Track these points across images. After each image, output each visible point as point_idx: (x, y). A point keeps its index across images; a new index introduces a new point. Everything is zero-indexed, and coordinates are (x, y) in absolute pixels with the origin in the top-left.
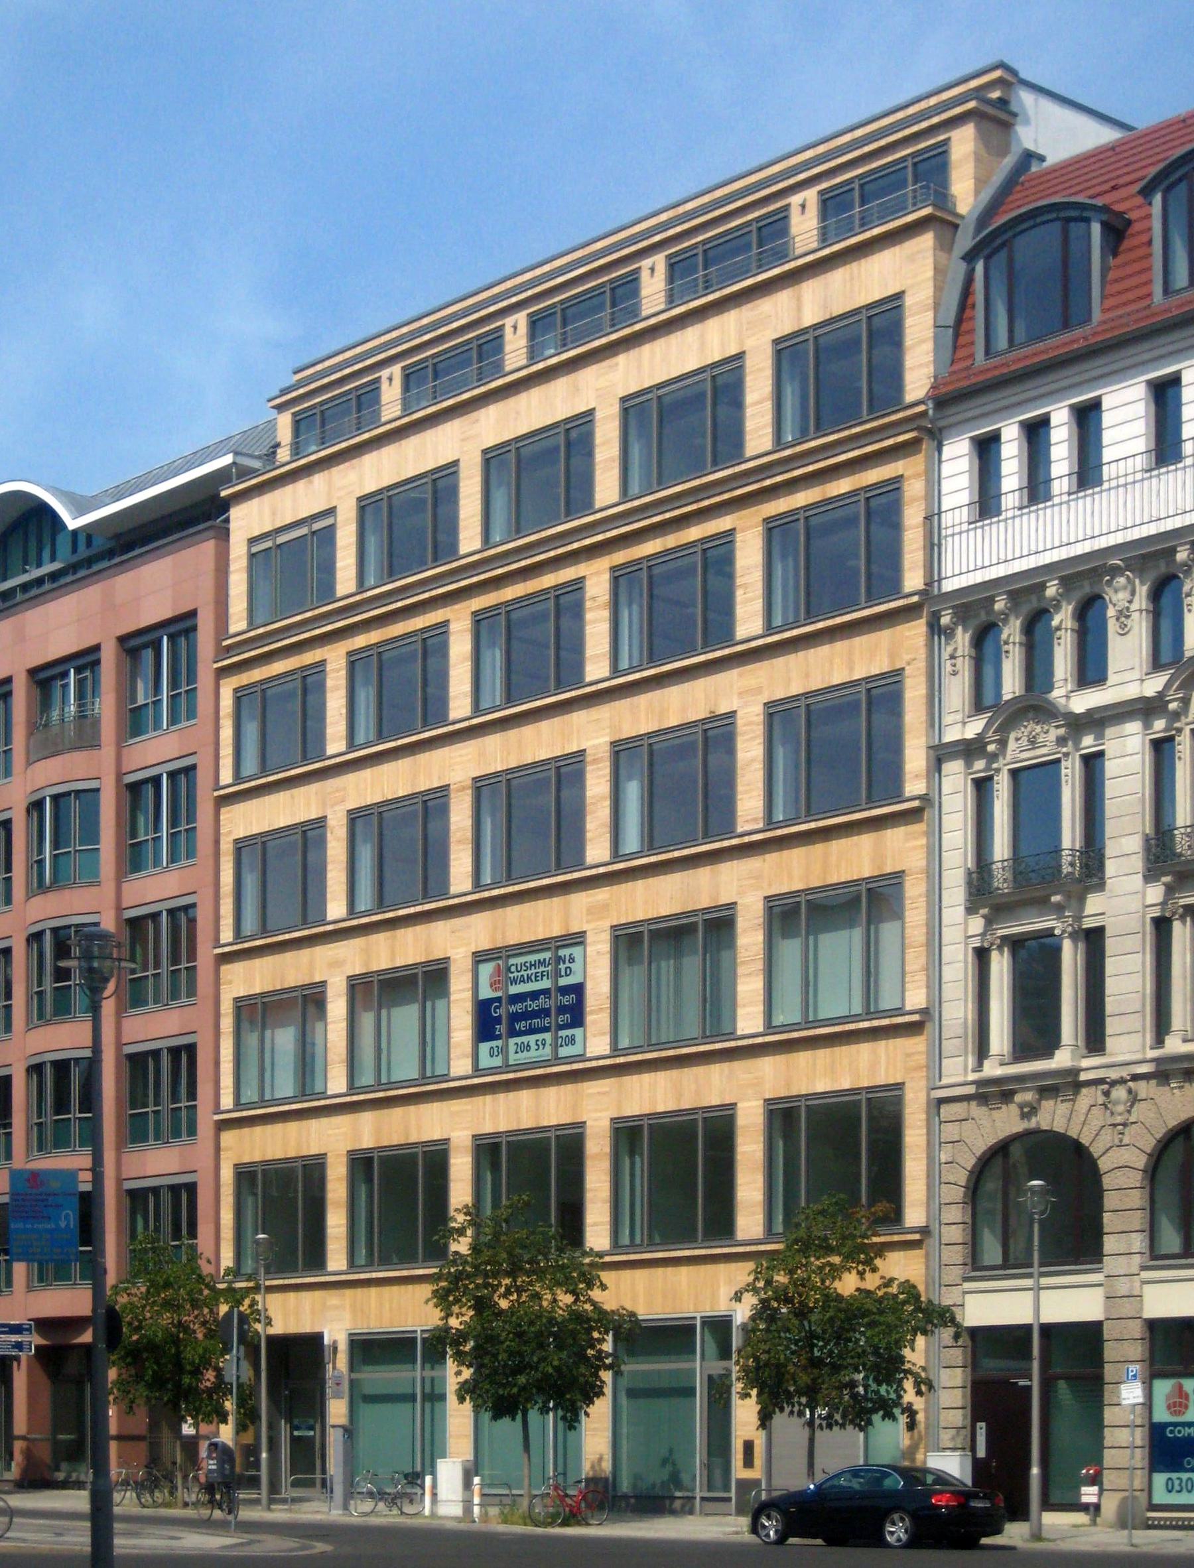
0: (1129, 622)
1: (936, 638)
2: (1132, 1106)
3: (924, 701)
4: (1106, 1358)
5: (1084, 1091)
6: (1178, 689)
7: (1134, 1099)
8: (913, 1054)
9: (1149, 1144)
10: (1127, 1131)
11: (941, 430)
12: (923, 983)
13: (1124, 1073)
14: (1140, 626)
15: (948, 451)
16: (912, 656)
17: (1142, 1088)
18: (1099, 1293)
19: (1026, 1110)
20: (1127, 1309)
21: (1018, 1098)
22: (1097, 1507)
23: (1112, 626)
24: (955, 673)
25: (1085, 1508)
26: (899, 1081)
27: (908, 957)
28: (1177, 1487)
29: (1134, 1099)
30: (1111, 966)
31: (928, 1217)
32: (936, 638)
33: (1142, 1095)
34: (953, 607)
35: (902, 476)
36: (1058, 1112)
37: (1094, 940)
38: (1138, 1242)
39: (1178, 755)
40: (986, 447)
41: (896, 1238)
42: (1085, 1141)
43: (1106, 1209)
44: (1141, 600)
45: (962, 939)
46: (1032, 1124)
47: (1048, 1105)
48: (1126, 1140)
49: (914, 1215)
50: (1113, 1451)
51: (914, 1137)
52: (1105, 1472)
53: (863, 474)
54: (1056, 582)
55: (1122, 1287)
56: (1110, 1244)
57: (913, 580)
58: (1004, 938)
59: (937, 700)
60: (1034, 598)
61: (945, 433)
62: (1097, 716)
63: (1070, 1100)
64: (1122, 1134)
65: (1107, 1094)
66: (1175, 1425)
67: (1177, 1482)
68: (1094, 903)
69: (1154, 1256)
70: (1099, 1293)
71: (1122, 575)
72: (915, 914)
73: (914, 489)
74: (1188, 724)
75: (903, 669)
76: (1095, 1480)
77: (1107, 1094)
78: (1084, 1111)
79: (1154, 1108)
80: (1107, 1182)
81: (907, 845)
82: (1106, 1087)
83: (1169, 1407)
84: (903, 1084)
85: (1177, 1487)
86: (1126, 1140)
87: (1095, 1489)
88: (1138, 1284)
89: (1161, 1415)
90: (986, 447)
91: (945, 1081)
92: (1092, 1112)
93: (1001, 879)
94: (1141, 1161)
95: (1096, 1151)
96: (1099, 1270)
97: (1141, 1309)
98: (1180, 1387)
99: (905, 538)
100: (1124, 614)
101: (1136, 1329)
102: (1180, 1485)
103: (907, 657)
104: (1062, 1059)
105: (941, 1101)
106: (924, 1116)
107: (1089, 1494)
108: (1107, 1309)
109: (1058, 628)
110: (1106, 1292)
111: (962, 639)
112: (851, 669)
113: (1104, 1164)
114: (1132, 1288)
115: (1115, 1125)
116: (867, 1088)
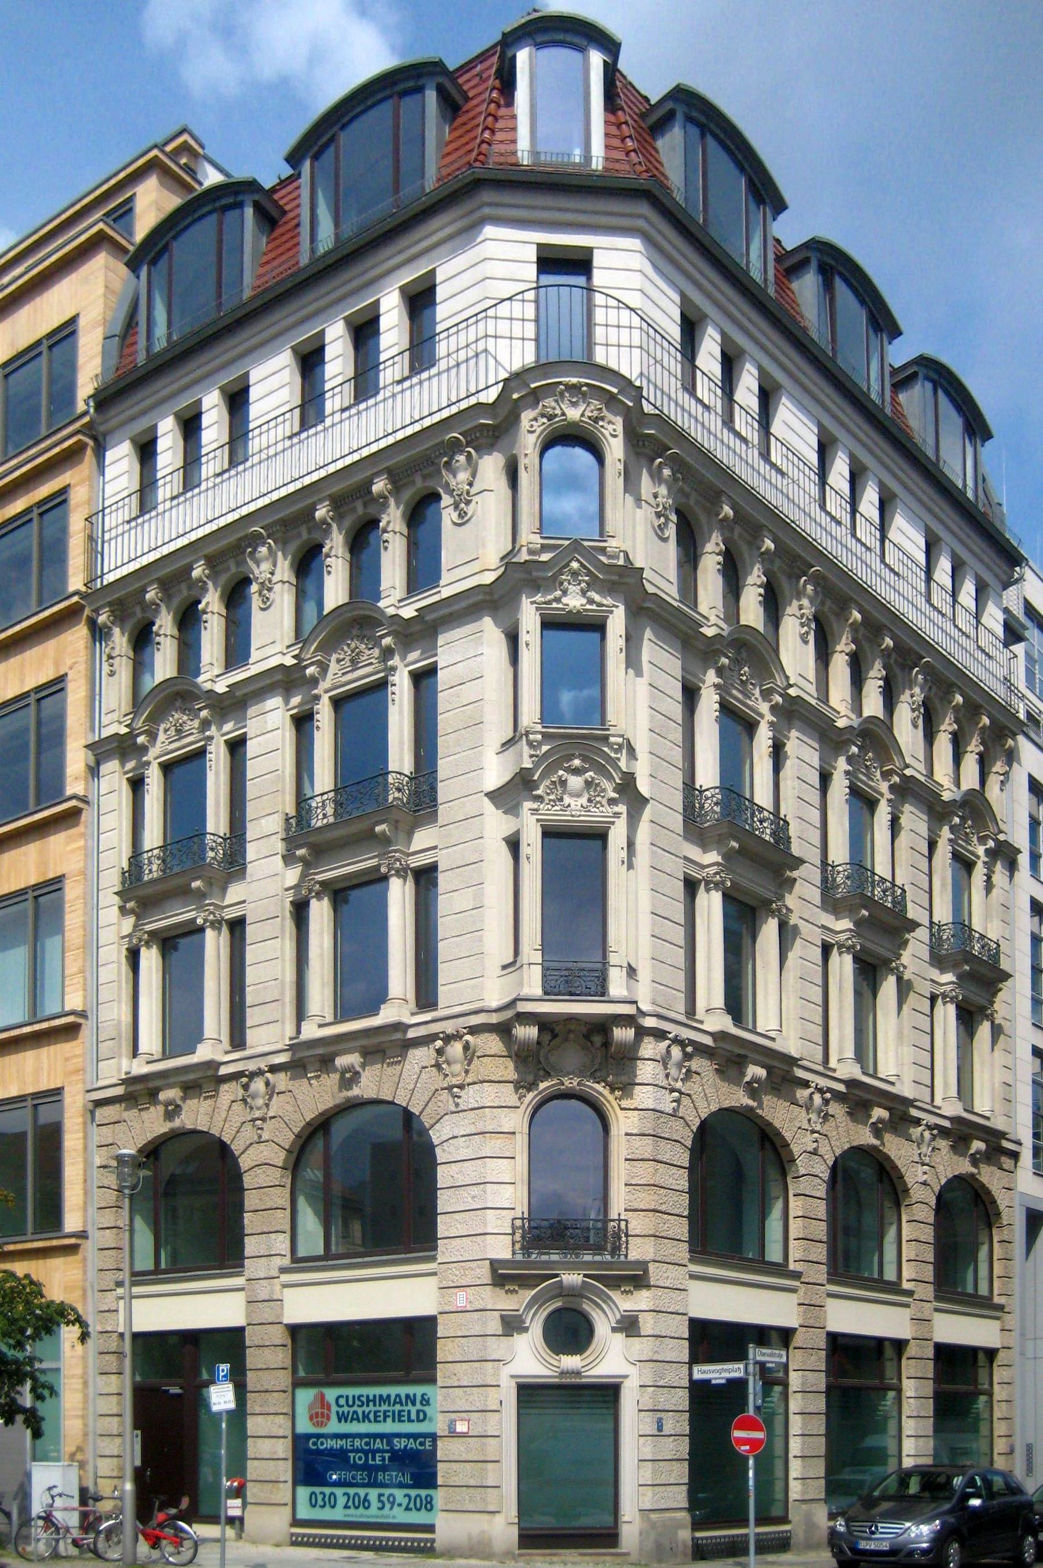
0: (271, 596)
1: (98, 644)
2: (270, 1099)
3: (83, 703)
4: (248, 1366)
5: (225, 1087)
6: (315, 651)
7: (271, 1091)
8: (72, 1058)
9: (287, 1138)
10: (265, 1126)
11: (105, 435)
12: (80, 986)
13: (262, 1064)
14: (284, 599)
15: (110, 455)
16: (74, 660)
17: (281, 1080)
18: (240, 1298)
19: (170, 1108)
20: (266, 1313)
21: (163, 1096)
22: (241, 1519)
23: (256, 602)
24: (112, 674)
25: (231, 1521)
26: (59, 1086)
27: (67, 961)
28: (320, 1502)
29: (271, 1091)
30: (251, 954)
31: (85, 1222)
32: (98, 644)
33: (281, 1086)
34: (110, 604)
35: (69, 485)
36: (202, 1110)
37: (237, 926)
38: (281, 1243)
39: (316, 724)
40: (146, 451)
41: (55, 1243)
42: (226, 1139)
43: (247, 1208)
44: (285, 569)
45: (116, 939)
46: (177, 1123)
47: (191, 1104)
48: (265, 1137)
49: (72, 1222)
50: (256, 1463)
51: (72, 1141)
52: (249, 1485)
53: (36, 492)
54: (202, 562)
55: (263, 1291)
56: (251, 1246)
57: (76, 582)
58: (152, 934)
59: (97, 703)
60: (184, 586)
61: (108, 438)
62: (239, 693)
63: (212, 1097)
64: (262, 1129)
65: (246, 1087)
66: (318, 1436)
67: (320, 1497)
68: (235, 892)
69: (295, 1259)
70: (240, 1298)
71: (264, 544)
72: (73, 919)
73: (78, 496)
74: (326, 692)
75: (66, 674)
76: (239, 1492)
77: (246, 1087)
78: (226, 1107)
79: (292, 1101)
80: (248, 1181)
81: (68, 848)
82: (244, 1080)
83: (311, 1418)
84: (63, 1088)
85: (320, 1502)
86: (265, 1136)
87: (238, 1502)
88: (278, 1287)
89: (305, 1426)
90: (146, 451)
91: (101, 1083)
92: (233, 1108)
93: (152, 871)
94: (279, 1157)
95: (236, 1148)
96: (239, 1274)
97: (282, 1315)
98: (323, 1396)
99: (71, 545)
100: (266, 587)
101: (279, 1336)
102: (323, 1499)
103: (69, 662)
104: (203, 1053)
105: (99, 1103)
106: (80, 1120)
107: (233, 1507)
108: (248, 1315)
109: (205, 612)
110: (247, 1296)
111: (120, 641)
112: (22, 681)
113: (245, 1162)
114: (272, 1291)
115: (253, 1120)
116: (32, 1094)
